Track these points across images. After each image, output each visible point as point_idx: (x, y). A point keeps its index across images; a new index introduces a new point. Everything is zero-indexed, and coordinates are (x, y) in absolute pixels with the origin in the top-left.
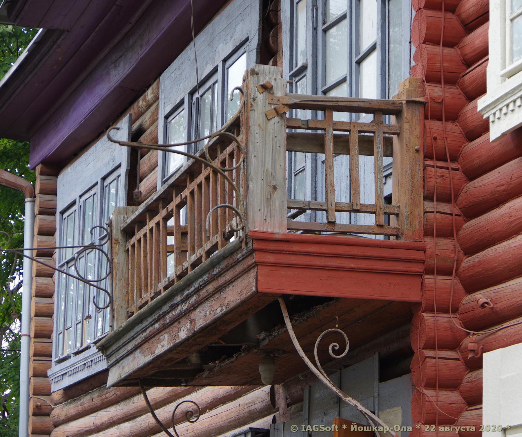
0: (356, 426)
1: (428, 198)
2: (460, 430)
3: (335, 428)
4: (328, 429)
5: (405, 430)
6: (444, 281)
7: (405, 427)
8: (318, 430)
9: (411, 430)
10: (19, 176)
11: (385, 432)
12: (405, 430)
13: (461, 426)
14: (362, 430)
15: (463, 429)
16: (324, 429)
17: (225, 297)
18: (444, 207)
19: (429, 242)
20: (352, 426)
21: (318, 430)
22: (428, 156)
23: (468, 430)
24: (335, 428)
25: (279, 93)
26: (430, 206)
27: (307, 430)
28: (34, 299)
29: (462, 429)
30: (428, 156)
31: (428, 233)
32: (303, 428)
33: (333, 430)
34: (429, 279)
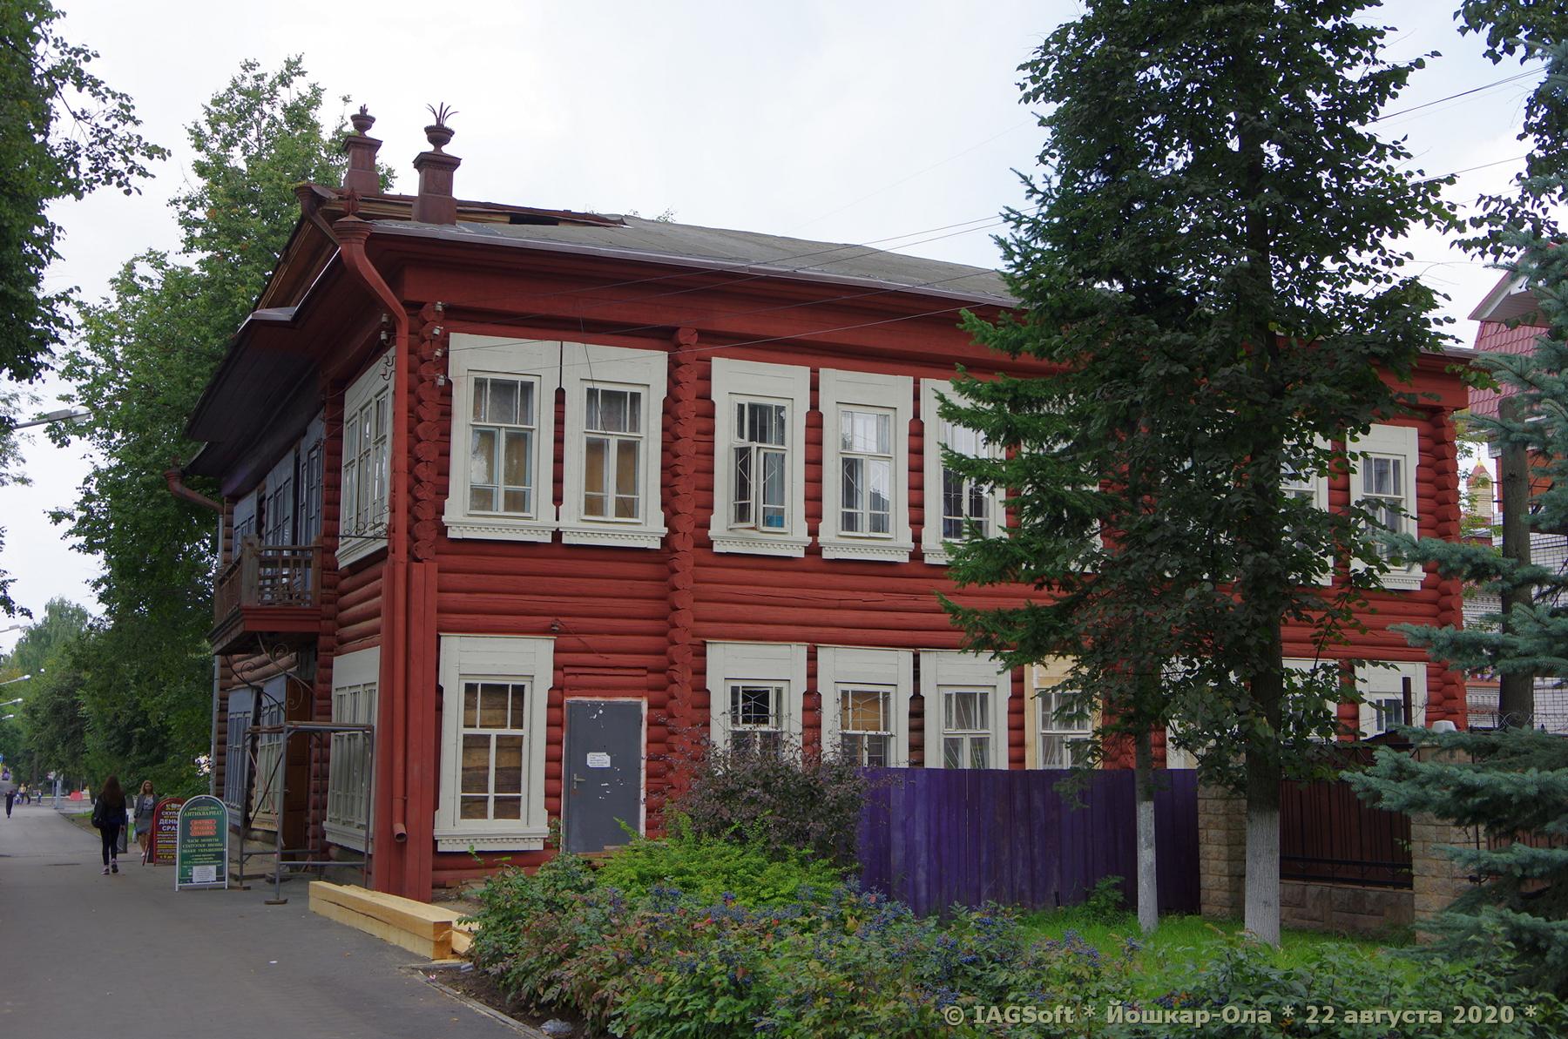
0: (1119, 1009)
1: (323, 587)
2: (1400, 1021)
3: (1063, 1015)
4: (1045, 1016)
5: (1253, 1020)
6: (330, 623)
7: (1253, 1013)
8: (1017, 1020)
9: (1269, 1021)
10: (130, 267)
11: (1198, 1025)
12: (1253, 1020)
13: (1404, 1009)
14: (1136, 1020)
15: (1410, 1016)
16: (1034, 1016)
17: (1228, 628)
18: (330, 591)
19: (323, 607)
20: (1110, 1008)
21: (1017, 1020)
22: (324, 569)
23: (1422, 1020)
24: (1063, 1015)
25: (256, 546)
26: (324, 591)
27: (988, 1020)
28: (1403, 496)
29: (1405, 1018)
30: (324, 569)
31: (322, 602)
32: (979, 1015)
33: (1058, 1020)
34: (323, 623)
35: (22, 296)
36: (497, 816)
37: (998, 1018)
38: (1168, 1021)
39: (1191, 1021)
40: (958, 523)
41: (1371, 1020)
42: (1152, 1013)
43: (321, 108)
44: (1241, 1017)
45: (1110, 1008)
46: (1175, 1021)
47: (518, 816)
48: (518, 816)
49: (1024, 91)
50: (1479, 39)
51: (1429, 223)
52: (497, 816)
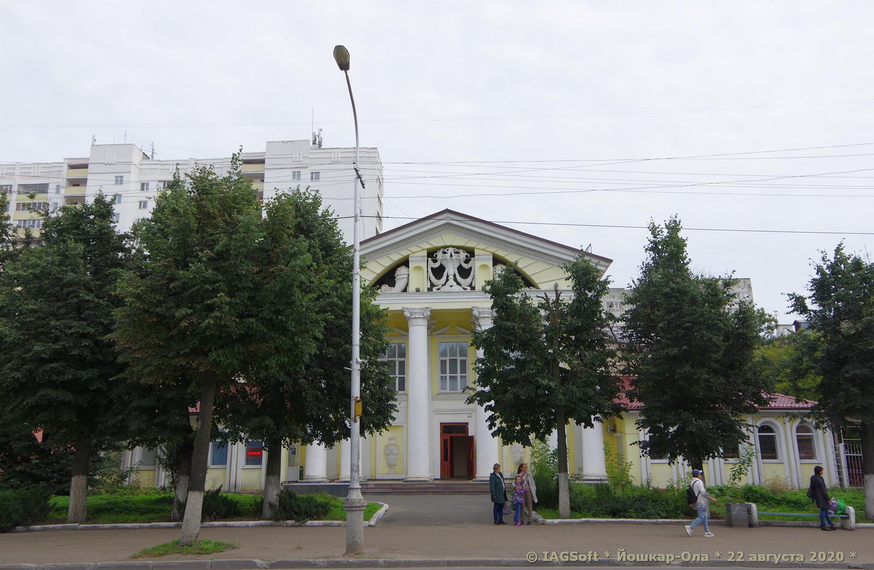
5: (698, 559)
7: (698, 555)
8: (567, 560)
35: (775, 333)
36: (759, 436)
37: (556, 558)
38: (651, 560)
39: (663, 560)
40: (461, 356)
41: (764, 560)
42: (642, 555)
43: (126, 231)
44: (691, 558)
45: (619, 553)
46: (655, 560)
47: (247, 463)
48: (247, 463)
49: (75, 191)
50: (686, 242)
51: (148, 219)
52: (759, 436)
